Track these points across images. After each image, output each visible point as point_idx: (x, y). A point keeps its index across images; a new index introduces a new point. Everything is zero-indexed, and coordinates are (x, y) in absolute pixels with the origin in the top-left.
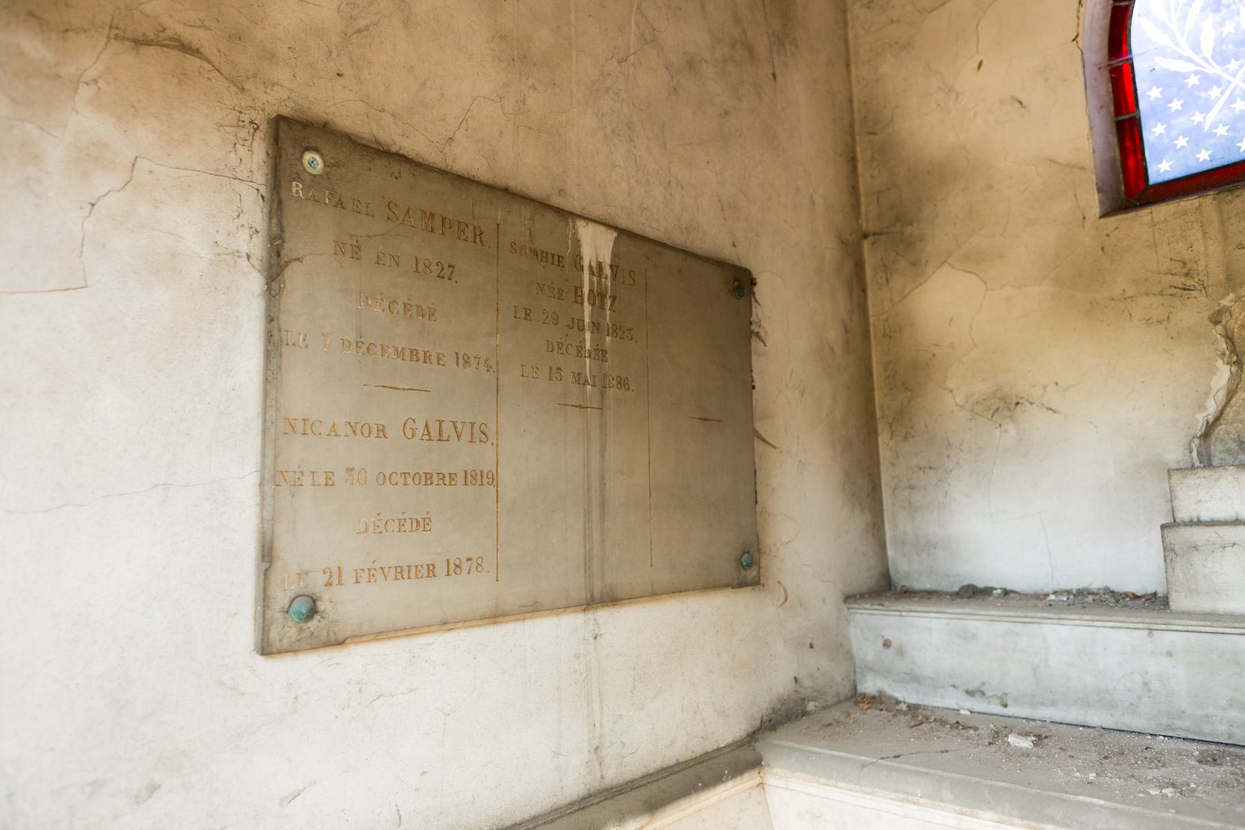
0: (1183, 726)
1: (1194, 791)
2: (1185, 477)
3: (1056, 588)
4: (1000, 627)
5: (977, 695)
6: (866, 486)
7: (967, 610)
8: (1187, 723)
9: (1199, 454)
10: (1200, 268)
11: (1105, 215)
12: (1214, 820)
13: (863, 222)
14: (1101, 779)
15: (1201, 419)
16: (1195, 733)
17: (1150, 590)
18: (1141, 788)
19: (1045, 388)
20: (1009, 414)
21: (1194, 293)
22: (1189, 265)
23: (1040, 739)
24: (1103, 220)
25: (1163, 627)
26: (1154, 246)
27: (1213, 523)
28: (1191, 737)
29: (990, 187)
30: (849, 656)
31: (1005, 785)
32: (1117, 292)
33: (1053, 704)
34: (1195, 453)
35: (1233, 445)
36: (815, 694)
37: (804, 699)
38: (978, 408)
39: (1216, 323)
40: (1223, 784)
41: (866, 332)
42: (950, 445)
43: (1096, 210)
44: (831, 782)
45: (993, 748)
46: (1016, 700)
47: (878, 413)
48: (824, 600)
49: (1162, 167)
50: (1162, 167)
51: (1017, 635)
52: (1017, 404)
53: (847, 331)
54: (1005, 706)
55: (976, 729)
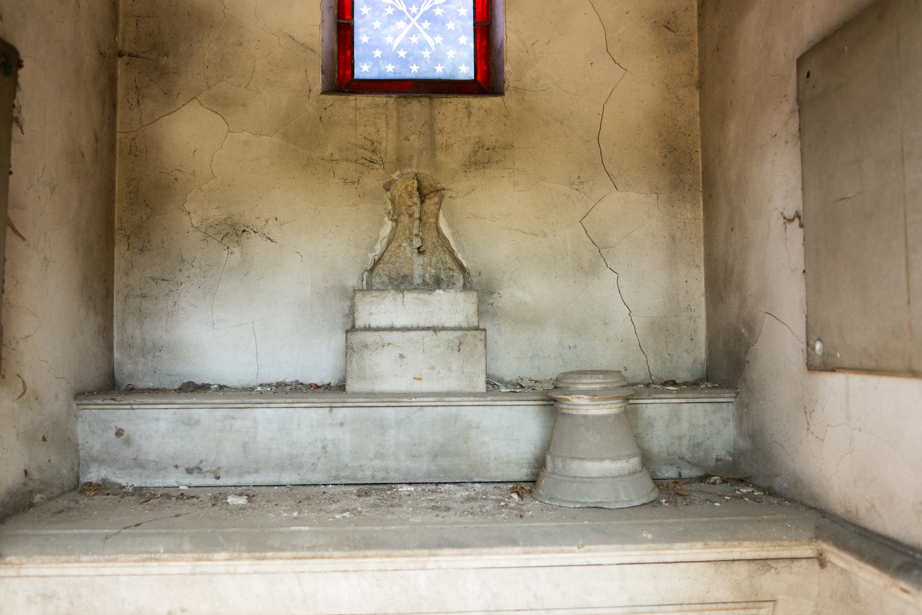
0: (345, 475)
1: (360, 512)
2: (364, 296)
3: (259, 382)
4: (220, 413)
5: (195, 472)
6: (100, 293)
7: (194, 400)
8: (348, 473)
9: (367, 284)
10: (382, 149)
11: (324, 93)
12: (378, 526)
13: (119, 39)
14: (302, 515)
15: (371, 257)
16: (353, 479)
17: (326, 382)
18: (329, 515)
19: (267, 221)
20: (237, 239)
21: (377, 166)
22: (376, 144)
23: (250, 498)
24: (323, 96)
25: (340, 405)
26: (355, 125)
27: (378, 329)
28: (349, 482)
29: (241, 44)
30: (76, 448)
31: (235, 529)
32: (327, 154)
33: (257, 471)
34: (365, 282)
35: (386, 279)
36: (42, 486)
37: (31, 492)
38: (211, 231)
39: (388, 190)
40: (375, 506)
41: (113, 145)
42: (183, 261)
43: (319, 87)
44: (73, 558)
45: (216, 508)
46: (227, 472)
47: (117, 225)
48: (57, 396)
49: (363, 70)
50: (363, 70)
51: (233, 418)
52: (244, 231)
53: (97, 141)
54: (218, 478)
55: (197, 498)
